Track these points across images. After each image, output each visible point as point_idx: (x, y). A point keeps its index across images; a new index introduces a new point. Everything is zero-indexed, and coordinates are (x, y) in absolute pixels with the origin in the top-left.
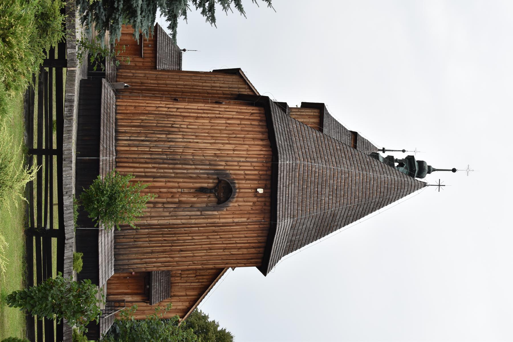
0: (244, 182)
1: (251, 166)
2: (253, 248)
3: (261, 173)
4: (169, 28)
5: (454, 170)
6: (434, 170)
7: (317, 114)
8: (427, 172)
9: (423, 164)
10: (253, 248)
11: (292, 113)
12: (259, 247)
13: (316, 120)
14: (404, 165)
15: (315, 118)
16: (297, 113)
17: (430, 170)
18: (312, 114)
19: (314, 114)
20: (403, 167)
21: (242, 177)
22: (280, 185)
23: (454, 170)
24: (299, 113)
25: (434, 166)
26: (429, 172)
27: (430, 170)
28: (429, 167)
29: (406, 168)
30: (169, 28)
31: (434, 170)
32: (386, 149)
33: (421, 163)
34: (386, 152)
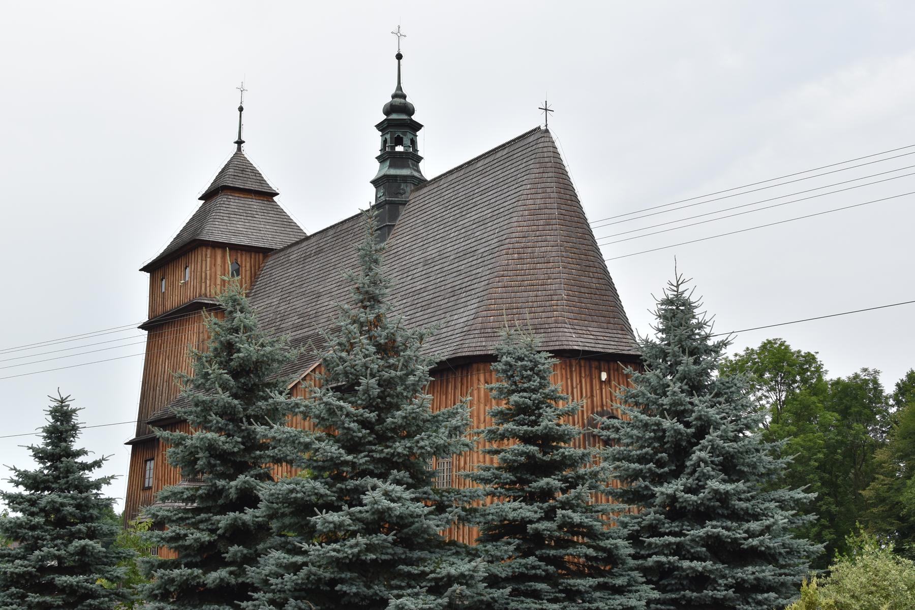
0: (595, 399)
1: (577, 387)
2: (571, 372)
3: (583, 375)
4: (749, 528)
5: (399, 57)
6: (399, 88)
7: (209, 252)
8: (402, 100)
9: (395, 105)
10: (571, 372)
11: (208, 295)
12: (580, 367)
13: (219, 253)
14: (399, 136)
15: (215, 256)
16: (208, 285)
17: (399, 94)
18: (208, 260)
19: (208, 256)
20: (402, 138)
21: (589, 401)
22: (599, 348)
23: (399, 57)
24: (208, 282)
25: (393, 90)
26: (404, 97)
27: (399, 94)
28: (394, 96)
29: (405, 133)
30: (749, 528)
31: (399, 88)
32: (236, 139)
33: (389, 110)
34: (243, 139)
